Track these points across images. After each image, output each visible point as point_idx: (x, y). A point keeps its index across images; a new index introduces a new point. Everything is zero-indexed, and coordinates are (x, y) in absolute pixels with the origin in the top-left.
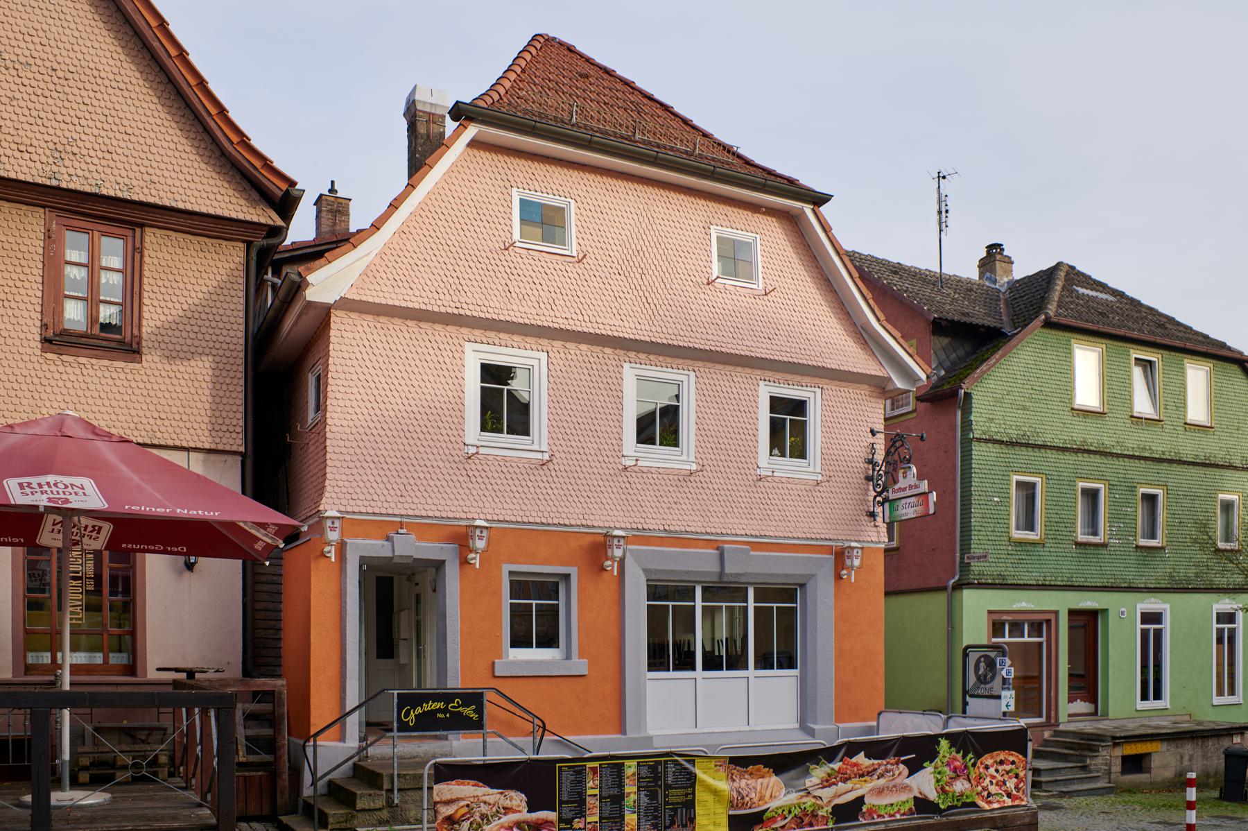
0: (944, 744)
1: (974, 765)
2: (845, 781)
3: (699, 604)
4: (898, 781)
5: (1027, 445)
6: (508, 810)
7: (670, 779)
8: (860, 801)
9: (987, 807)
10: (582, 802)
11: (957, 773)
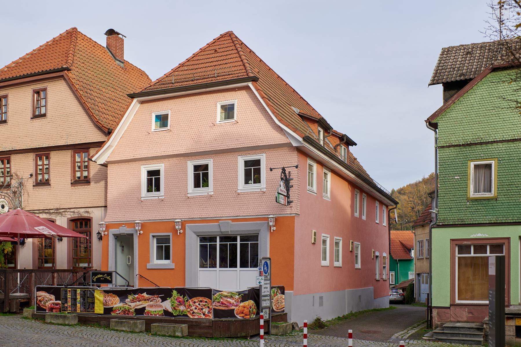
0: (175, 293)
1: (187, 301)
2: (139, 301)
3: (218, 243)
4: (158, 303)
5: (481, 144)
6: (51, 300)
7: (88, 295)
8: (144, 308)
9: (191, 317)
10: (67, 299)
11: (181, 303)
